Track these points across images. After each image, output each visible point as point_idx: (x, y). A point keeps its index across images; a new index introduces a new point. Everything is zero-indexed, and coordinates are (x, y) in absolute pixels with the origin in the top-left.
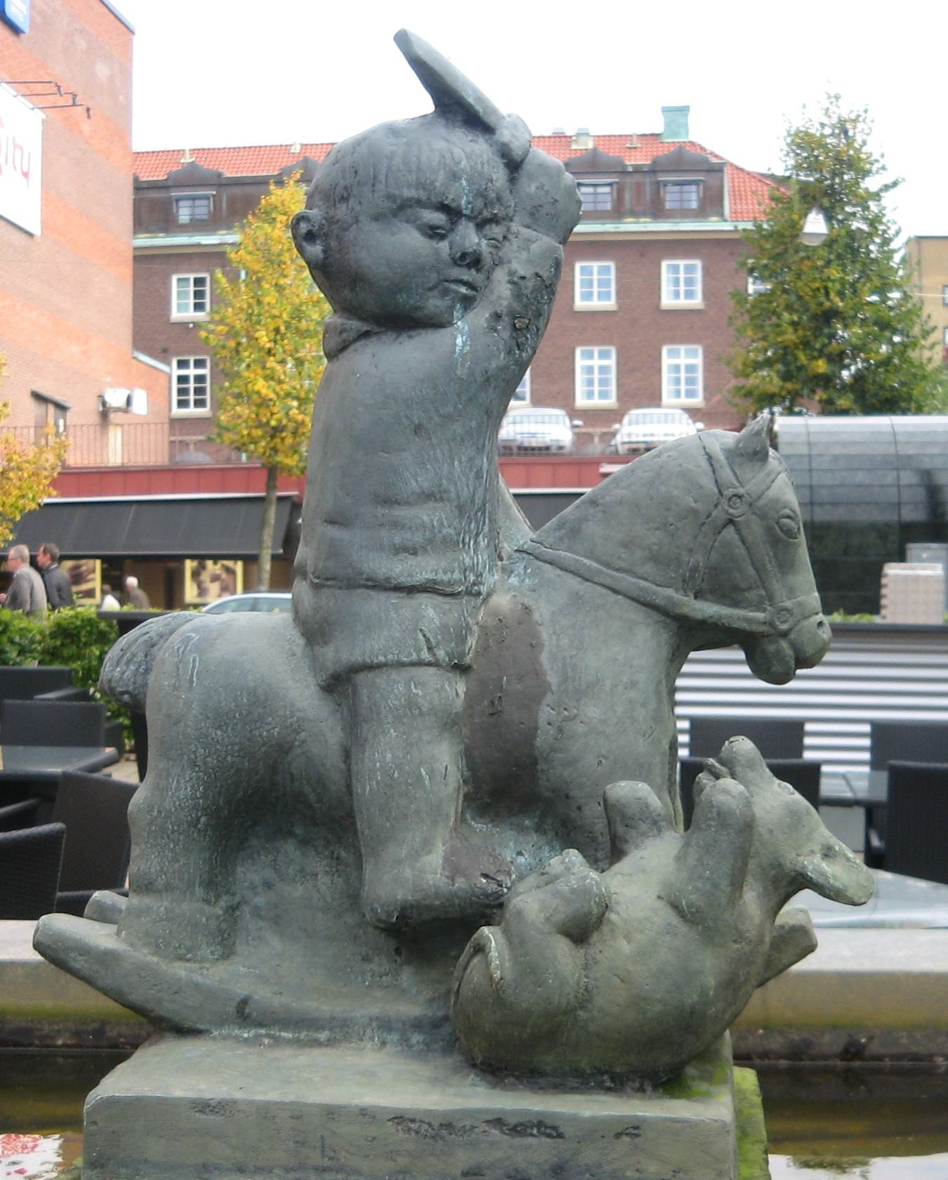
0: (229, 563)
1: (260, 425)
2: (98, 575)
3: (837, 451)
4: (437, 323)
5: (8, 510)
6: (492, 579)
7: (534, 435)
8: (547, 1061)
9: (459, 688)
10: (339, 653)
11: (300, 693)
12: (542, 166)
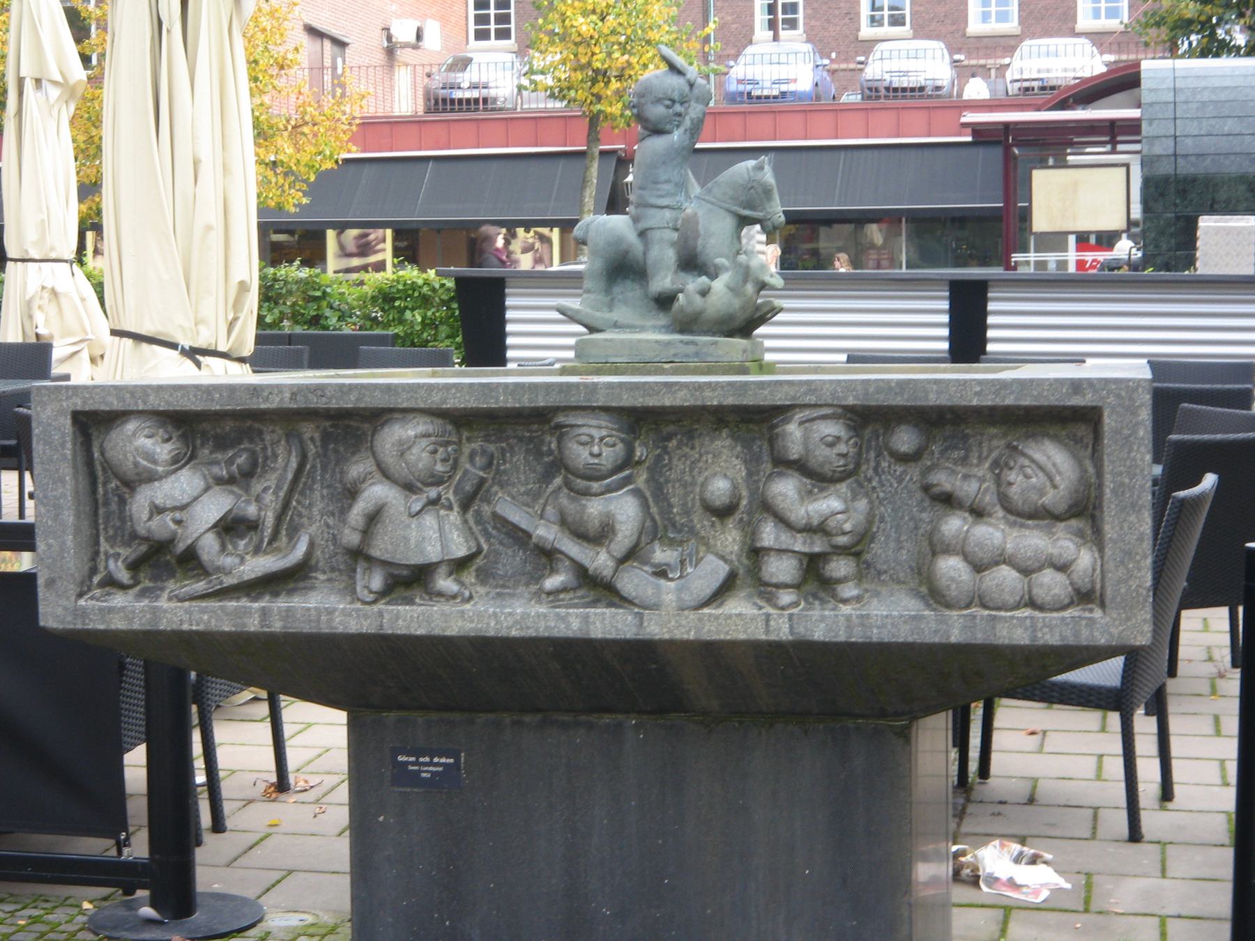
0: (545, 231)
1: (580, 67)
2: (389, 245)
3: (1206, 96)
4: (669, 132)
5: (303, 169)
6: (686, 205)
7: (906, 73)
8: (695, 328)
9: (675, 235)
10: (643, 225)
11: (631, 237)
12: (700, 85)
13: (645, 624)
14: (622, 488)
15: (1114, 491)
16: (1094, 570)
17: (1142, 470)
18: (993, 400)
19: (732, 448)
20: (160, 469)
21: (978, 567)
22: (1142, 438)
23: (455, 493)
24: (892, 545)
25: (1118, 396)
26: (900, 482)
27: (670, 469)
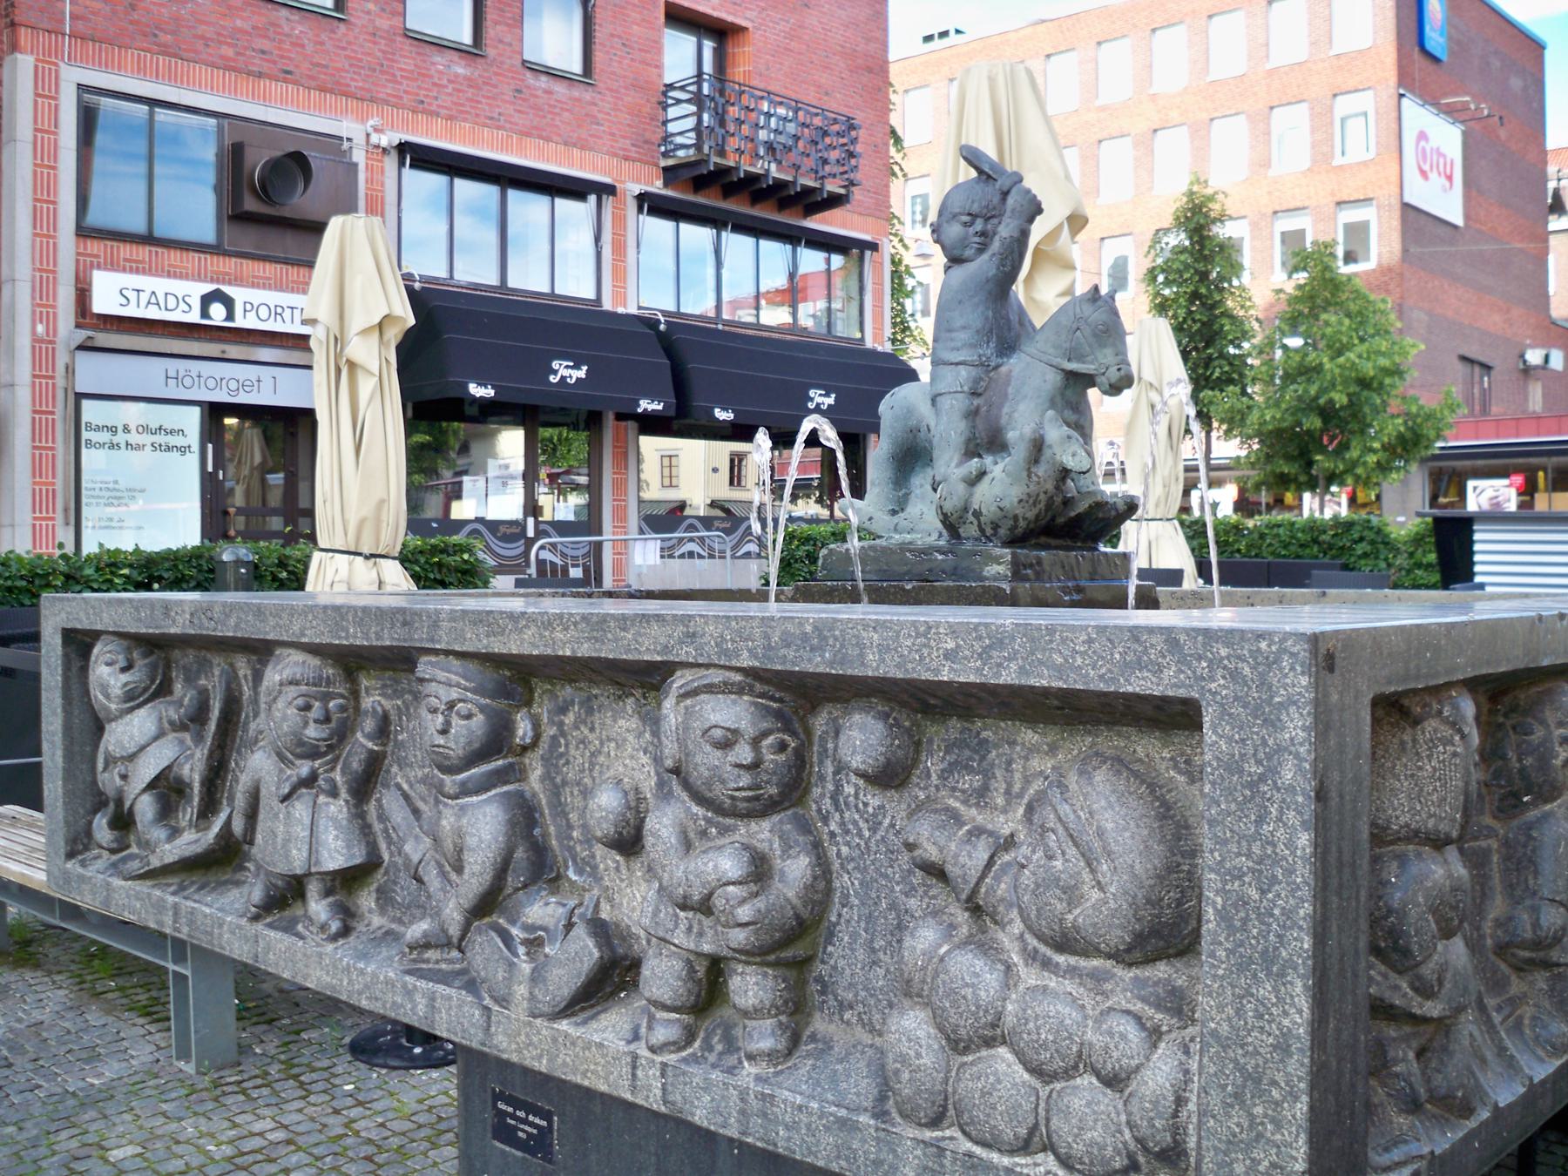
13: (493, 1029)
14: (487, 790)
15: (1223, 916)
16: (1180, 1101)
17: (1290, 872)
18: (979, 671)
19: (640, 735)
20: (113, 706)
21: (958, 1044)
22: (1291, 789)
23: (343, 772)
24: (861, 954)
25: (1234, 675)
26: (873, 830)
27: (568, 762)
